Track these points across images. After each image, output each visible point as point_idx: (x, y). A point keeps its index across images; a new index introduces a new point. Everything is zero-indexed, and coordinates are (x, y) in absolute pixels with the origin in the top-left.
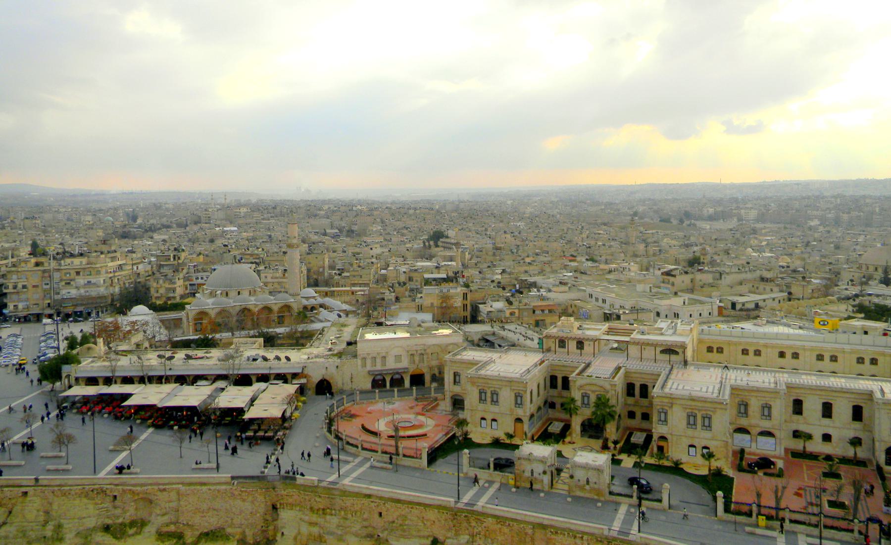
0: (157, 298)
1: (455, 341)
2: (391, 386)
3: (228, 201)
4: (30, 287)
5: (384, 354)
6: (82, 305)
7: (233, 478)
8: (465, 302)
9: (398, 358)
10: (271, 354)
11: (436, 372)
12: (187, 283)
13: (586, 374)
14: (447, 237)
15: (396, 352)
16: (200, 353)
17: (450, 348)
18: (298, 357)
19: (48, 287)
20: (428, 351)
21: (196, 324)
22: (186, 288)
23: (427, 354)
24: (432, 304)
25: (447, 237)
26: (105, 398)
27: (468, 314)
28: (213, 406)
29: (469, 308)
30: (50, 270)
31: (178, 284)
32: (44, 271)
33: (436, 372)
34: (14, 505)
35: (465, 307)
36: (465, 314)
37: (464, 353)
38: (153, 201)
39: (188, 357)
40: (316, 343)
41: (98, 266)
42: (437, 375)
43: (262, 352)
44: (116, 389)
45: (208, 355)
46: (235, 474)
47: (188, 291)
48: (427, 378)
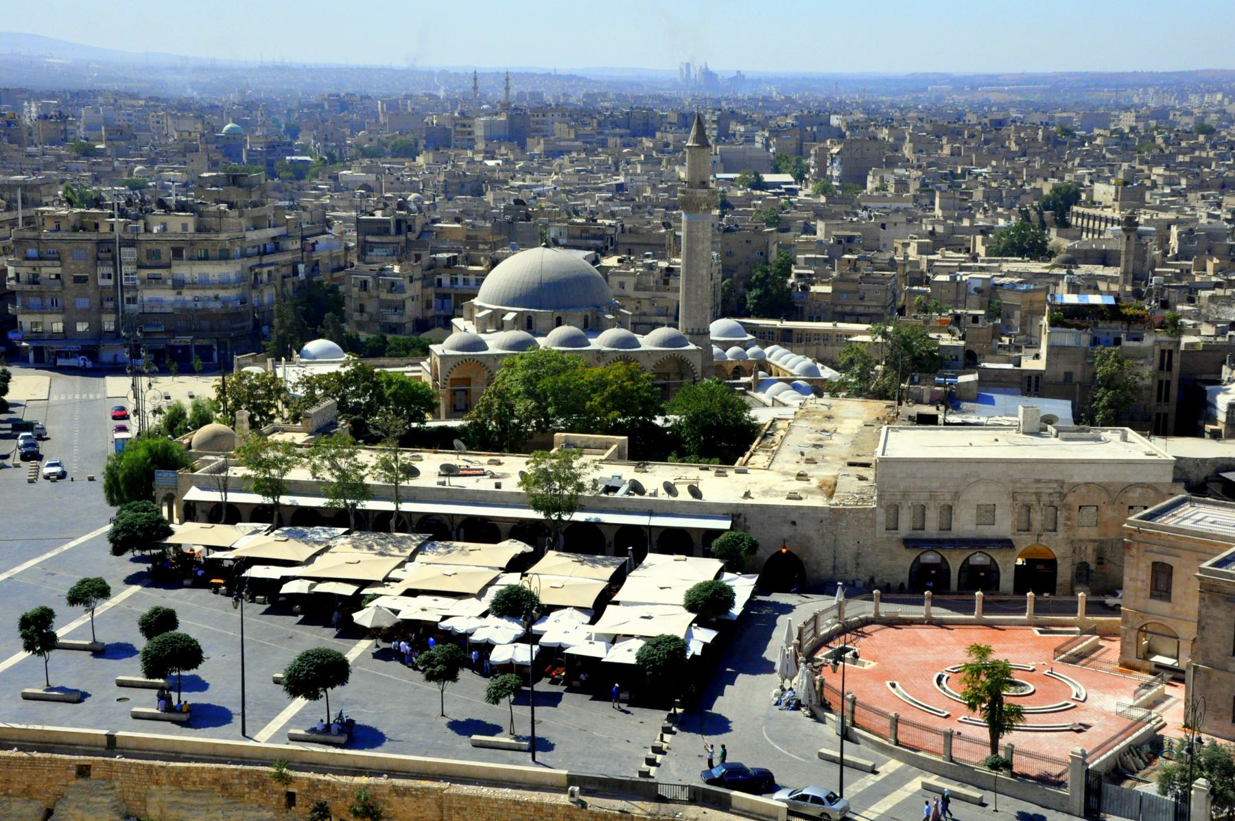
0: (360, 325)
1: (1151, 479)
2: (1020, 589)
3: (514, 92)
4: (69, 282)
5: (947, 499)
6: (187, 331)
7: (572, 780)
8: (1165, 376)
9: (987, 513)
10: (655, 477)
11: (1090, 557)
12: (430, 291)
13: (318, 548)
14: (1093, 204)
15: (979, 495)
16: (481, 460)
17: (1135, 495)
18: (721, 486)
19: (111, 282)
20: (1070, 499)
21: (454, 393)
22: (429, 306)
23: (1068, 507)
24: (1068, 376)
25: (1093, 204)
26: (854, 318)
27: (1171, 408)
28: (118, 508)
29: (1174, 391)
30: (112, 241)
31: (409, 294)
32: (100, 242)
33: (1090, 557)
34: (60, 797)
35: (1163, 388)
36: (1163, 409)
37: (1187, 510)
38: (333, 90)
39: (449, 470)
40: (760, 459)
41: (223, 236)
42: (1093, 567)
43: (628, 472)
44: (167, 715)
45: (496, 470)
46: (577, 772)
47: (431, 313)
48: (1064, 572)
